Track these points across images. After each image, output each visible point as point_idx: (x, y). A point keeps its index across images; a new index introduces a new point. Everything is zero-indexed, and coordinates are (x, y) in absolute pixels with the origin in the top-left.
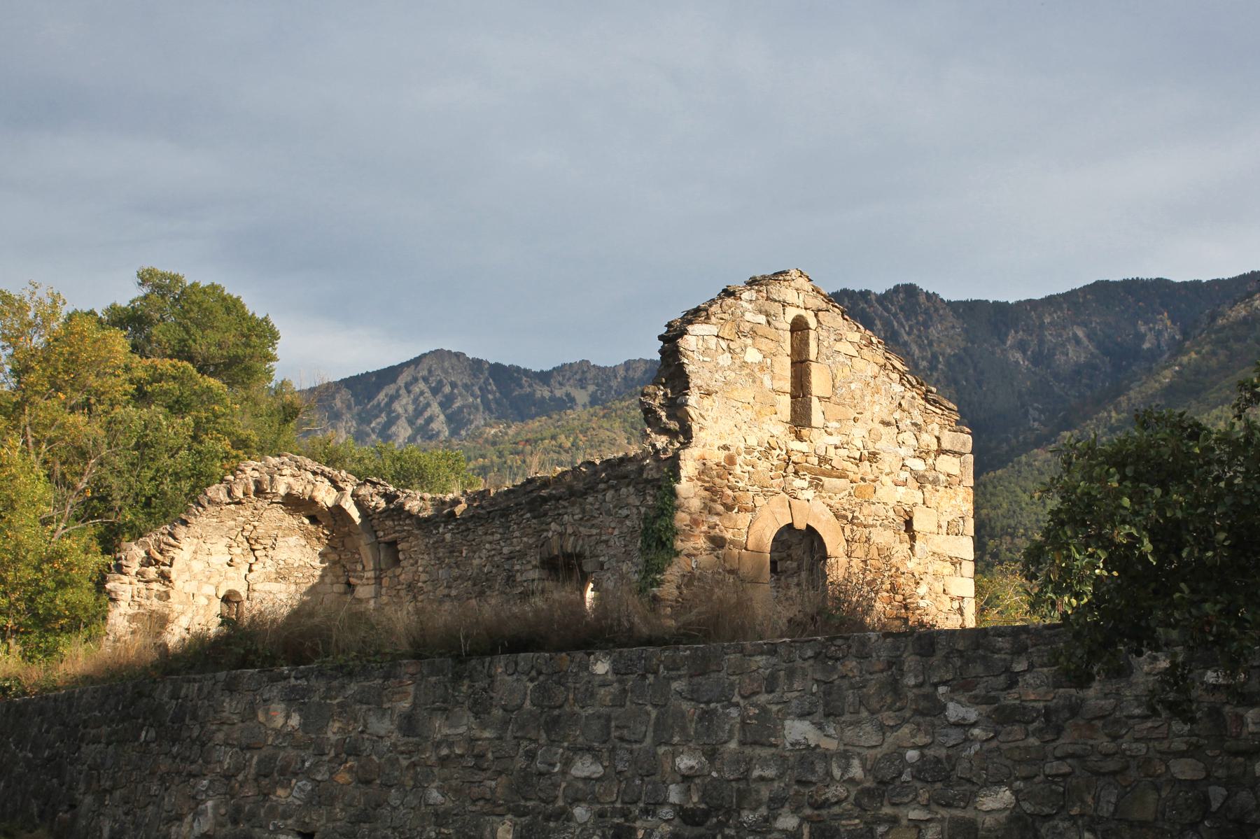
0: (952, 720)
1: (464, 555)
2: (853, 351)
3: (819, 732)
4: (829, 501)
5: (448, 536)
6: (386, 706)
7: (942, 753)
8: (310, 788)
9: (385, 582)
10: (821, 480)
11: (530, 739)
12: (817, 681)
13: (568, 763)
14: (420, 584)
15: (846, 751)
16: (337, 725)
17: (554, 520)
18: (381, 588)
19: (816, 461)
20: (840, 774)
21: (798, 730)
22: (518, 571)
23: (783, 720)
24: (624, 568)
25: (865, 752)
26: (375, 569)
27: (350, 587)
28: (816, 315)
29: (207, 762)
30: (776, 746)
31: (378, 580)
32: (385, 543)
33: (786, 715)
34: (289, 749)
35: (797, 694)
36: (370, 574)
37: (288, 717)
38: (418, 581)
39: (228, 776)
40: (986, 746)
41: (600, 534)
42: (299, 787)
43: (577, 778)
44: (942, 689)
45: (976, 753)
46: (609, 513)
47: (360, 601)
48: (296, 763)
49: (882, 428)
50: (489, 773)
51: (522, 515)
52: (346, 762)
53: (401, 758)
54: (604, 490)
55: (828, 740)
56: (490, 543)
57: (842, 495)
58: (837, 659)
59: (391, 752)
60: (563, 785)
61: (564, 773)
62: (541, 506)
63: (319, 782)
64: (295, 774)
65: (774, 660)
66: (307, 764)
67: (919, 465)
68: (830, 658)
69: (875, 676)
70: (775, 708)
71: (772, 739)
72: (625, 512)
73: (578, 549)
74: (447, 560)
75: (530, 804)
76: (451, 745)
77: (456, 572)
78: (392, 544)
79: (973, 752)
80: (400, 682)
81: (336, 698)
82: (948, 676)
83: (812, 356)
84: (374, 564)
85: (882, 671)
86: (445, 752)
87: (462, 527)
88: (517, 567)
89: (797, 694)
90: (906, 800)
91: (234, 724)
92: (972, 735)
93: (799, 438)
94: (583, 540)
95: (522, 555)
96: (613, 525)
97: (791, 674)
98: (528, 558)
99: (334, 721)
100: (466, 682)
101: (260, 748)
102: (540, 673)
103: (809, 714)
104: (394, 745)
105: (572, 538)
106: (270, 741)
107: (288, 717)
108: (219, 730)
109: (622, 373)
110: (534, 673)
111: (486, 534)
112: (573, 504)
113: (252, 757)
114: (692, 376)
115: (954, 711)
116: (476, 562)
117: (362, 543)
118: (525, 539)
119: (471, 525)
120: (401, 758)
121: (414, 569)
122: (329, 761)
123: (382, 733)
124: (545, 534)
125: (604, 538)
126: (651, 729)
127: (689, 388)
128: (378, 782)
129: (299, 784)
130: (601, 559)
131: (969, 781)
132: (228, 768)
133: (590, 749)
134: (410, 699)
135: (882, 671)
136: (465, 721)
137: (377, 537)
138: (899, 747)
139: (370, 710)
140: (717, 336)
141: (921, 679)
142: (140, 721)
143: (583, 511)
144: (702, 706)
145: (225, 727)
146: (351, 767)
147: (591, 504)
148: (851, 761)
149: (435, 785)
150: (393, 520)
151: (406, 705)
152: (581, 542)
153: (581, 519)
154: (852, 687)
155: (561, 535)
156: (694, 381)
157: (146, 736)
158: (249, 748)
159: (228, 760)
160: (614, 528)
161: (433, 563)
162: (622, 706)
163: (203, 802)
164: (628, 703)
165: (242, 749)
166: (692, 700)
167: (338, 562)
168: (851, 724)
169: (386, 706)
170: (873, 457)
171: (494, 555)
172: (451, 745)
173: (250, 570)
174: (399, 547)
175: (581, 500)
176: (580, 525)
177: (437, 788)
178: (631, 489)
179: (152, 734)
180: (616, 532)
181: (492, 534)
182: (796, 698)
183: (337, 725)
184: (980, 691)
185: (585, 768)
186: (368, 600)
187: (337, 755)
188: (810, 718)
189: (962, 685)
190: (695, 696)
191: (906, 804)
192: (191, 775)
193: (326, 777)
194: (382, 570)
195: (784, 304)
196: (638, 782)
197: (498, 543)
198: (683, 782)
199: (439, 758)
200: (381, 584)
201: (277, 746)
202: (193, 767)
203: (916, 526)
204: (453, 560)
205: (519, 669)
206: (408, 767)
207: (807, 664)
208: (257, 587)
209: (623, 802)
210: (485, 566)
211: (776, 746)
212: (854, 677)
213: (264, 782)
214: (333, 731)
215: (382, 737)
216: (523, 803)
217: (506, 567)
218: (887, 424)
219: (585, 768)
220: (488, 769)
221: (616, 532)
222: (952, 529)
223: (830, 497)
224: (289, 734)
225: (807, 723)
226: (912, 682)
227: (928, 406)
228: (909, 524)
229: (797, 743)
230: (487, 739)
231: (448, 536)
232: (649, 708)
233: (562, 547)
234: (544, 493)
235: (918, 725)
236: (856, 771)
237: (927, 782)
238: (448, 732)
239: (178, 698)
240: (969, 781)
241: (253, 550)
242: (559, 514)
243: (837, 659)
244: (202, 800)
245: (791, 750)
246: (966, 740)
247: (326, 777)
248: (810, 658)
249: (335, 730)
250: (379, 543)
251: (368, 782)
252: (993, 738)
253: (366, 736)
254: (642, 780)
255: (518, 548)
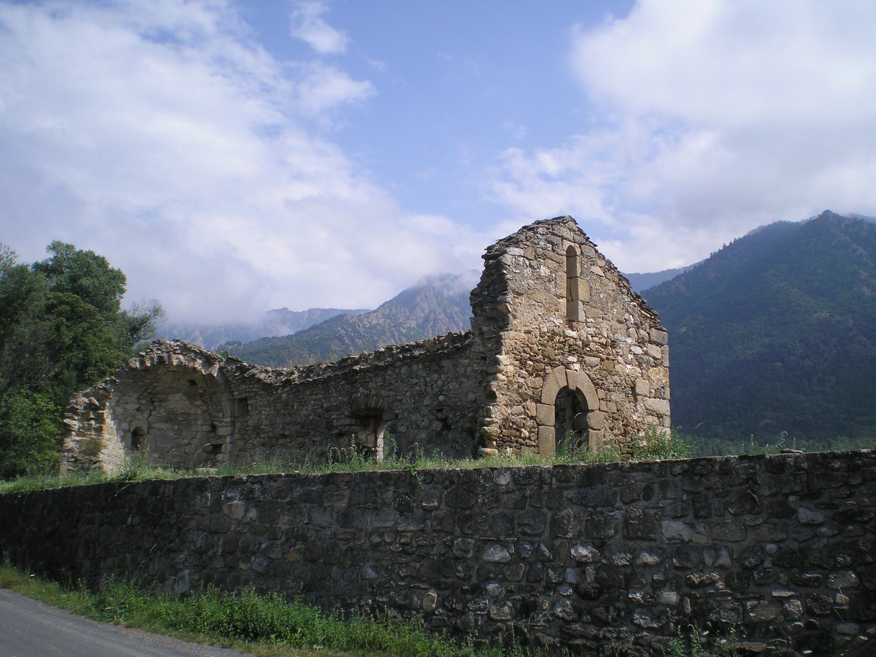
0: (803, 521)
1: (295, 408)
2: (601, 273)
3: (691, 530)
4: (588, 372)
5: (284, 396)
6: (326, 504)
7: (795, 546)
8: (266, 564)
9: (238, 425)
10: (584, 358)
11: (447, 532)
12: (686, 492)
13: (480, 550)
14: (263, 427)
15: (714, 544)
16: (286, 518)
17: (362, 386)
18: (235, 429)
19: (580, 343)
20: (711, 562)
21: (673, 528)
22: (334, 419)
23: (659, 520)
24: (414, 418)
25: (730, 545)
26: (231, 417)
27: (214, 428)
28: (580, 247)
29: (183, 542)
30: (655, 540)
31: (233, 423)
32: (239, 399)
33: (664, 516)
34: (248, 535)
35: (669, 501)
36: (228, 420)
37: (247, 511)
38: (261, 425)
39: (200, 553)
40: (832, 541)
41: (396, 395)
42: (257, 563)
43: (488, 562)
44: (792, 498)
45: (825, 546)
46: (403, 381)
47: (220, 437)
48: (255, 544)
49: (619, 325)
50: (414, 557)
51: (339, 383)
52: (295, 545)
53: (339, 543)
54: (400, 366)
55: (698, 536)
56: (314, 400)
57: (596, 368)
58: (702, 476)
59: (332, 539)
60: (476, 567)
61: (476, 558)
62: (353, 376)
63: (274, 559)
64: (254, 553)
65: (649, 476)
66: (263, 546)
67: (638, 350)
68: (696, 475)
69: (735, 488)
70: (652, 512)
71: (652, 535)
72: (415, 381)
73: (379, 405)
74: (282, 412)
75: (449, 580)
76: (381, 535)
77: (289, 419)
78: (244, 401)
79: (821, 545)
80: (337, 487)
81: (285, 498)
82: (797, 488)
83: (578, 275)
84: (231, 413)
85: (741, 485)
86: (376, 539)
87: (294, 390)
88: (334, 417)
89: (669, 501)
90: (769, 581)
91: (204, 515)
92: (820, 532)
93: (572, 328)
94: (383, 399)
95: (338, 408)
96: (406, 389)
97: (664, 486)
98: (343, 411)
99: (284, 515)
100: (392, 488)
101: (225, 533)
102: (452, 483)
103: (682, 516)
104: (335, 534)
105: (375, 398)
106: (233, 528)
107: (247, 511)
108: (192, 519)
109: (306, 315)
110: (447, 483)
111: (311, 394)
112: (376, 376)
113: (219, 539)
114: (509, 282)
115: (805, 514)
116: (304, 412)
117: (224, 399)
118: (340, 398)
119: (300, 388)
120: (339, 543)
121: (259, 416)
122: (282, 544)
123: (325, 524)
124: (355, 395)
125: (399, 398)
126: (548, 526)
127: (507, 290)
128: (322, 560)
129: (257, 560)
130: (397, 412)
131: (820, 567)
132: (201, 547)
133: (498, 541)
134: (346, 500)
135: (741, 485)
136: (392, 517)
137: (233, 396)
138: (759, 541)
139: (313, 507)
140: (524, 257)
141: (774, 491)
142: (126, 510)
143: (384, 380)
144: (590, 509)
145: (197, 517)
146: (300, 549)
147: (390, 375)
148: (720, 552)
149: (370, 564)
150: (246, 385)
151: (343, 504)
152: (381, 400)
153: (382, 385)
154: (717, 495)
155: (366, 396)
156: (511, 285)
157: (131, 521)
158: (216, 532)
159: (200, 541)
160: (406, 392)
161: (272, 413)
162: (524, 509)
163: (181, 570)
164: (527, 507)
165: (211, 534)
166: (581, 504)
167: (206, 411)
168: (718, 524)
169: (326, 504)
170: (614, 344)
171: (317, 408)
172: (381, 535)
173: (150, 415)
174: (249, 402)
175: (383, 373)
176: (381, 389)
177: (371, 567)
178: (420, 366)
179: (137, 519)
180: (408, 394)
181: (316, 394)
182: (669, 504)
183: (286, 518)
184: (824, 498)
185: (497, 554)
186: (225, 437)
187: (287, 540)
188: (683, 519)
189: (810, 495)
190: (583, 502)
191: (769, 584)
192: (170, 551)
193: (280, 556)
194: (235, 417)
195: (563, 238)
196: (540, 566)
197: (320, 400)
198: (578, 567)
199: (372, 545)
200: (234, 426)
201: (238, 532)
202: (172, 544)
203: (638, 390)
204: (287, 412)
205: (435, 479)
206: (346, 550)
207: (677, 479)
208: (154, 425)
209: (528, 580)
210: (310, 415)
211: (655, 540)
212: (718, 489)
213: (229, 558)
214: (283, 522)
215: (324, 528)
216: (443, 580)
217: (326, 416)
218: (620, 322)
219: (497, 554)
220: (413, 553)
221: (408, 394)
222: (658, 395)
223: (589, 369)
224: (248, 523)
225: (680, 523)
226: (767, 493)
227: (643, 312)
228: (633, 389)
229: (674, 538)
230: (412, 531)
231: (284, 396)
232: (545, 510)
233: (367, 403)
234: (357, 368)
235: (775, 525)
236: (724, 559)
237: (786, 568)
238: (379, 525)
239: (157, 495)
240: (820, 567)
241: (153, 402)
242: (366, 382)
243: (702, 476)
244: (180, 569)
245: (668, 544)
246: (815, 536)
247: (280, 556)
248: (679, 474)
249: (285, 521)
250: (234, 400)
251: (313, 561)
252: (837, 534)
253: (310, 526)
254: (543, 565)
255: (334, 404)
